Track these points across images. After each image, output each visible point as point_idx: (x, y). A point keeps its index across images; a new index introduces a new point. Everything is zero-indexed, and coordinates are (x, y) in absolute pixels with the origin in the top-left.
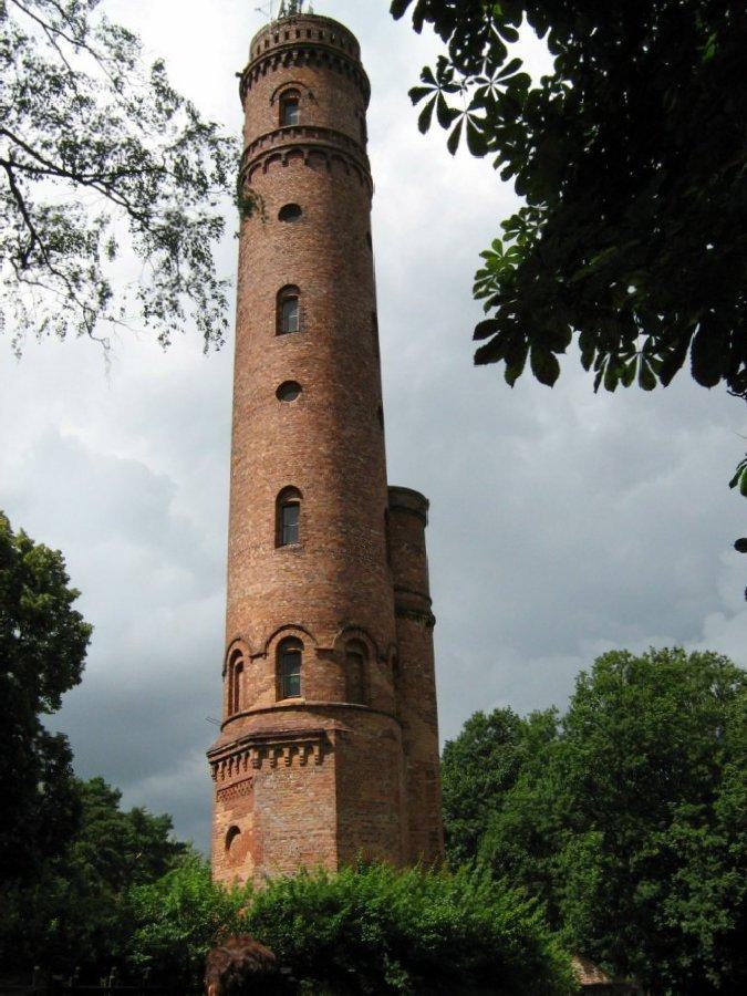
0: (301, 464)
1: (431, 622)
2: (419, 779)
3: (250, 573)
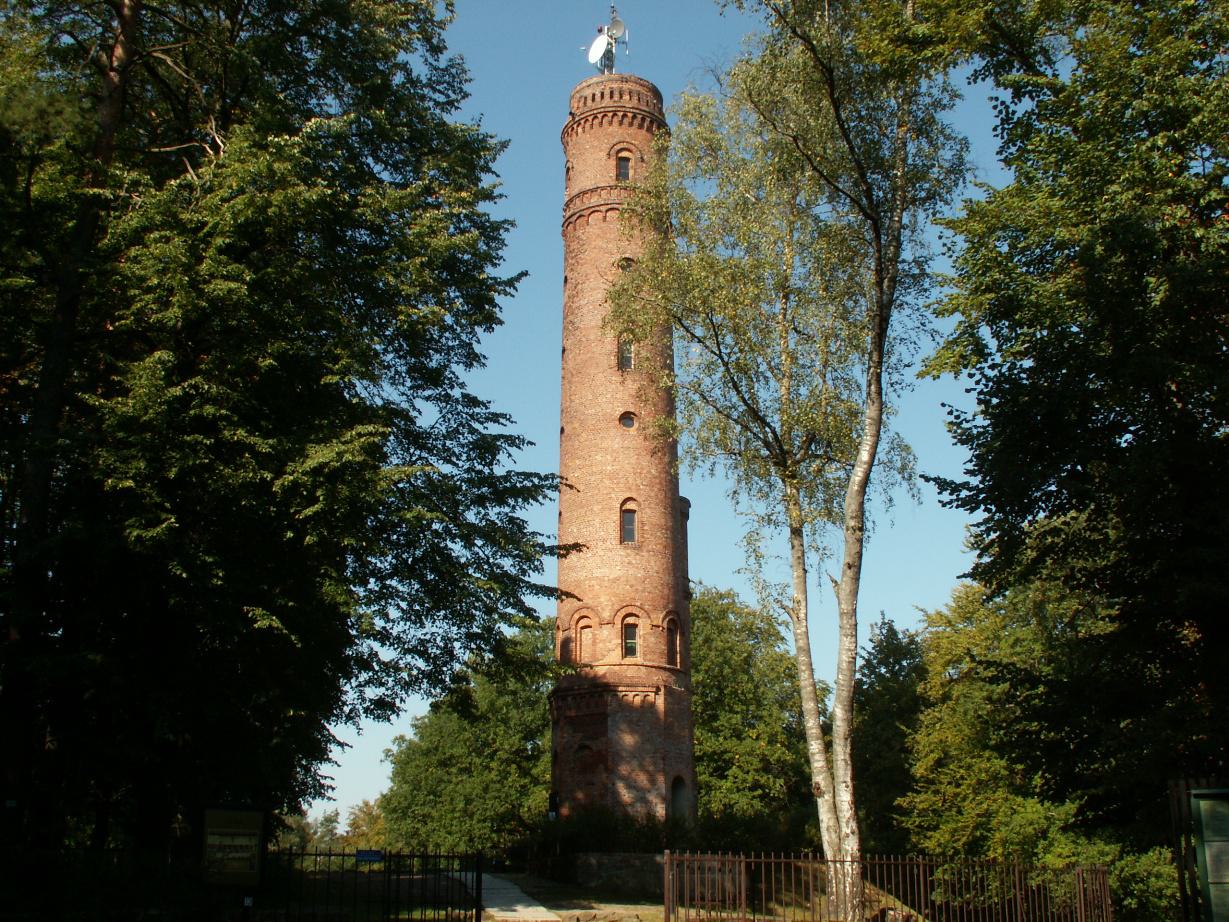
0: (639, 482)
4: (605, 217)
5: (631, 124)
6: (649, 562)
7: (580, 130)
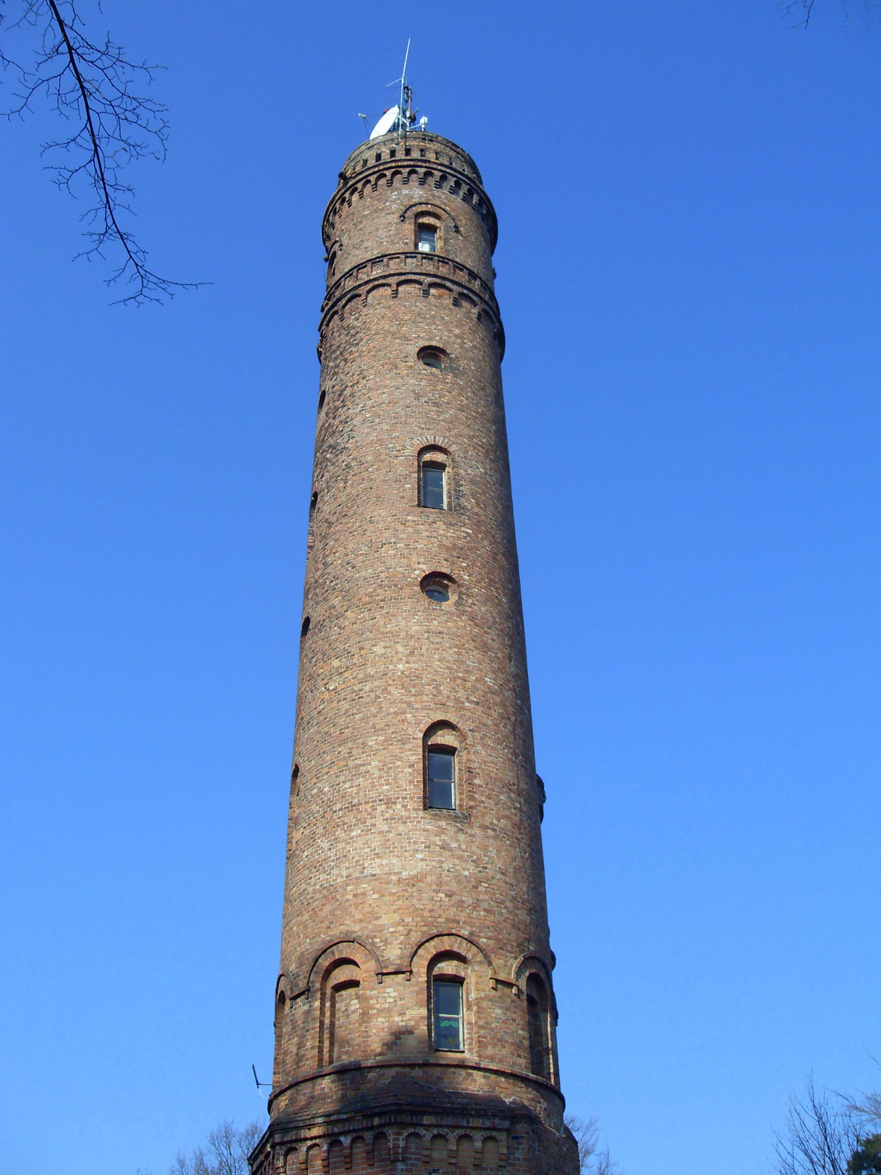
0: (461, 694)
3: (376, 841)
5: (439, 185)
6: (485, 849)
7: (355, 198)
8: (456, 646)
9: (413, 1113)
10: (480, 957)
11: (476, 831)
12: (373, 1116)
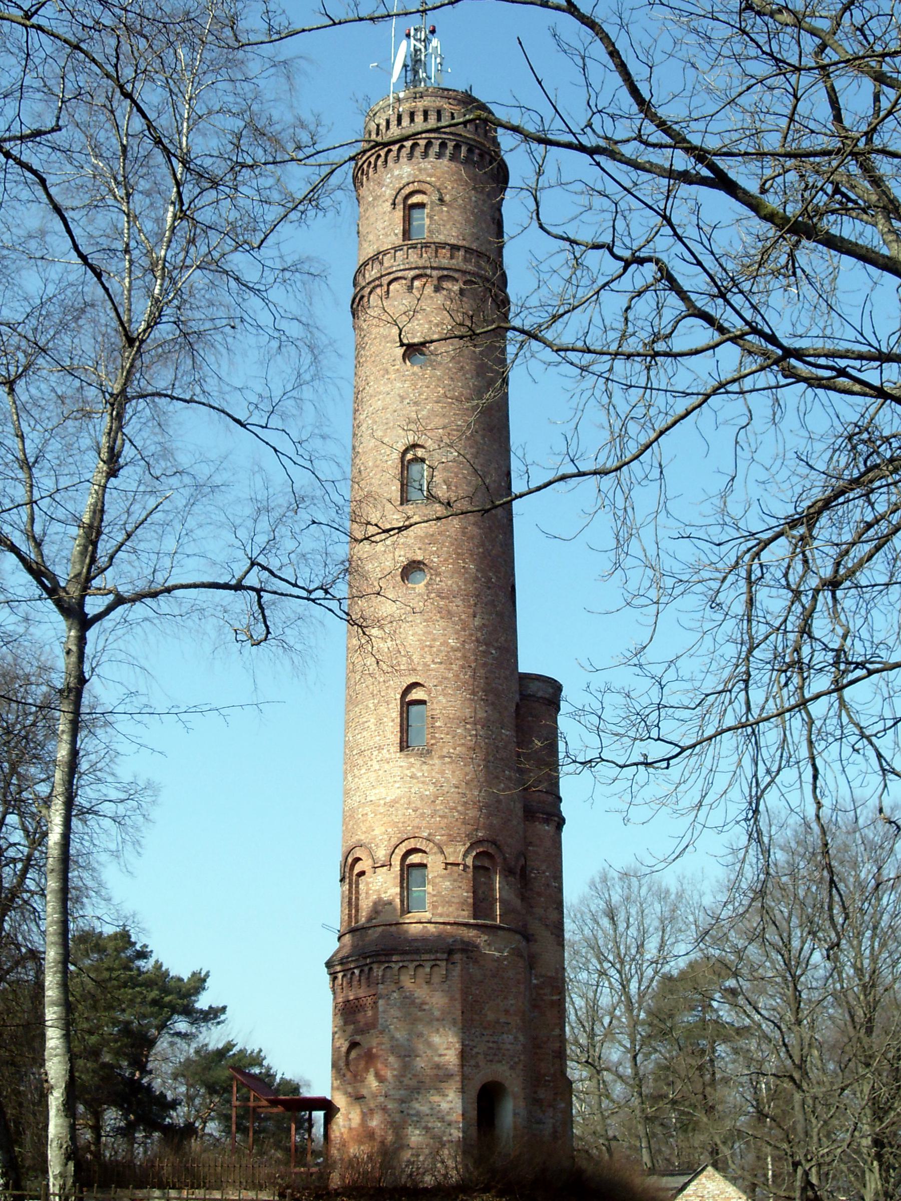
1: (561, 822)
2: (545, 994)
3: (372, 776)
4: (388, 292)
5: (425, 155)
8: (425, 621)
9: (386, 955)
10: (435, 849)
11: (436, 761)
12: (365, 958)
